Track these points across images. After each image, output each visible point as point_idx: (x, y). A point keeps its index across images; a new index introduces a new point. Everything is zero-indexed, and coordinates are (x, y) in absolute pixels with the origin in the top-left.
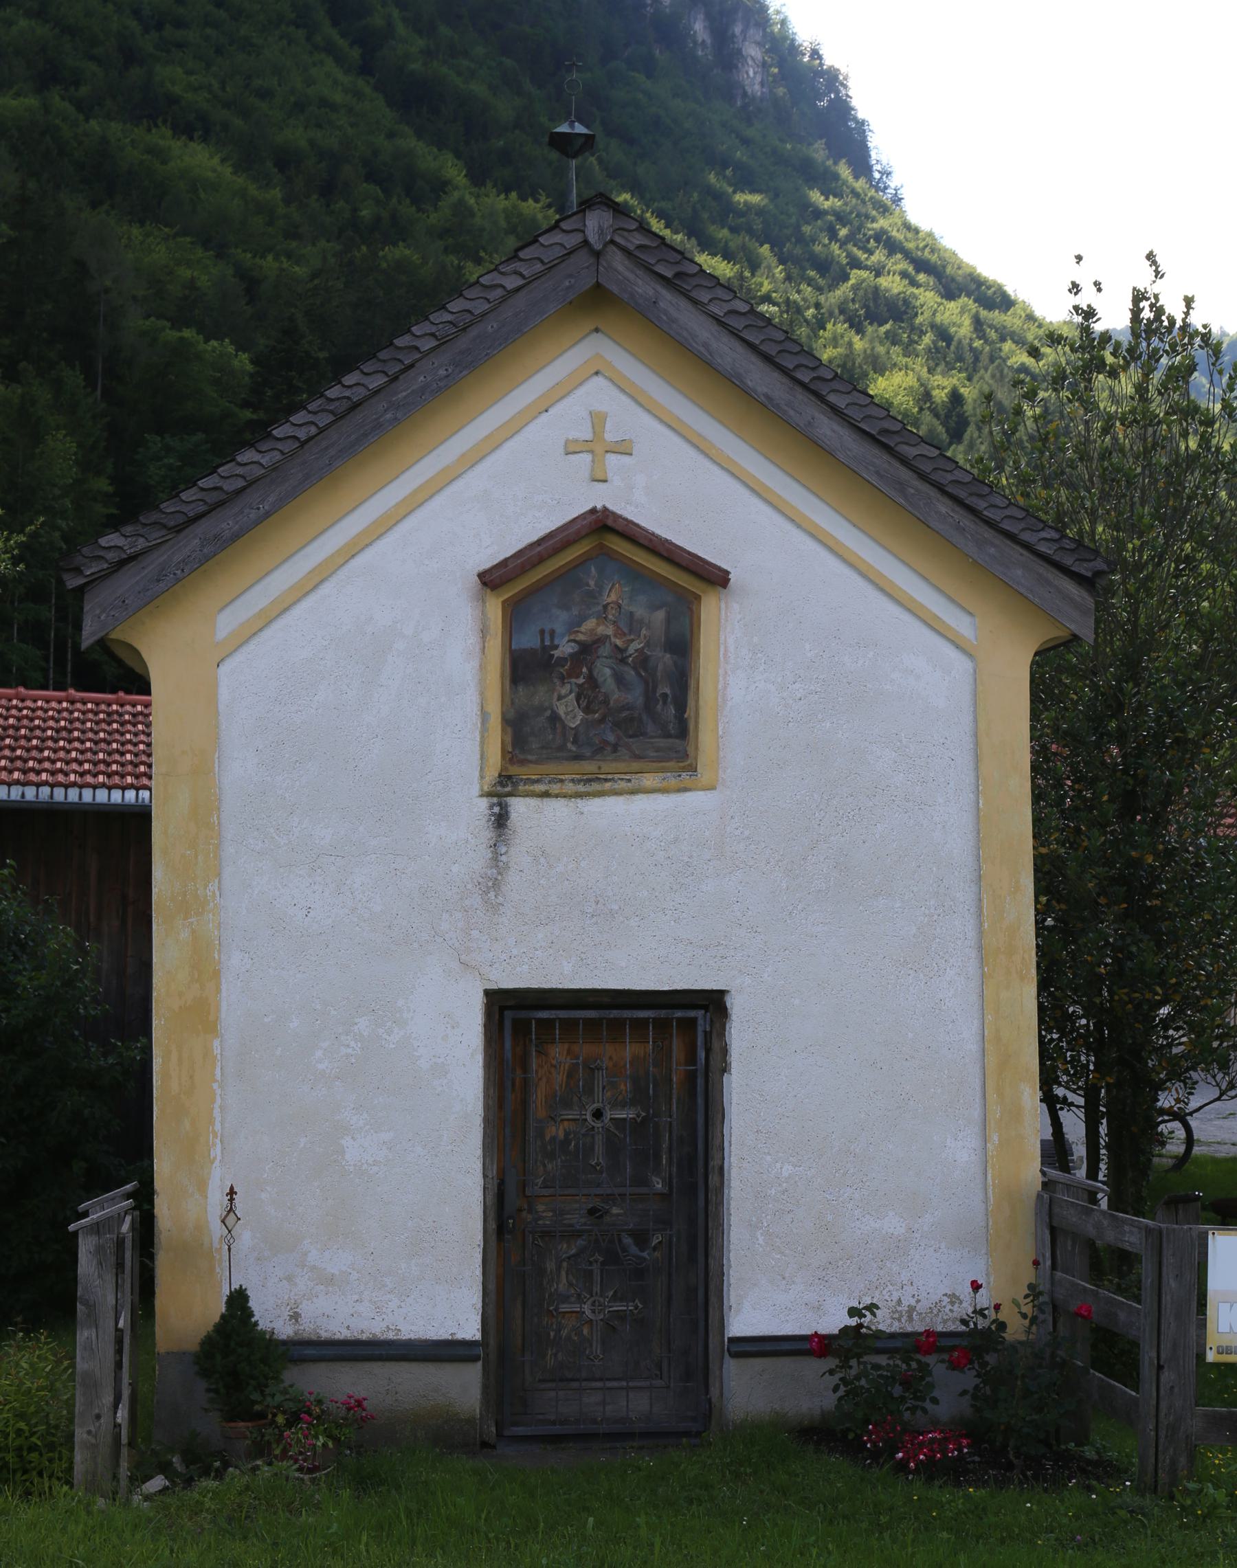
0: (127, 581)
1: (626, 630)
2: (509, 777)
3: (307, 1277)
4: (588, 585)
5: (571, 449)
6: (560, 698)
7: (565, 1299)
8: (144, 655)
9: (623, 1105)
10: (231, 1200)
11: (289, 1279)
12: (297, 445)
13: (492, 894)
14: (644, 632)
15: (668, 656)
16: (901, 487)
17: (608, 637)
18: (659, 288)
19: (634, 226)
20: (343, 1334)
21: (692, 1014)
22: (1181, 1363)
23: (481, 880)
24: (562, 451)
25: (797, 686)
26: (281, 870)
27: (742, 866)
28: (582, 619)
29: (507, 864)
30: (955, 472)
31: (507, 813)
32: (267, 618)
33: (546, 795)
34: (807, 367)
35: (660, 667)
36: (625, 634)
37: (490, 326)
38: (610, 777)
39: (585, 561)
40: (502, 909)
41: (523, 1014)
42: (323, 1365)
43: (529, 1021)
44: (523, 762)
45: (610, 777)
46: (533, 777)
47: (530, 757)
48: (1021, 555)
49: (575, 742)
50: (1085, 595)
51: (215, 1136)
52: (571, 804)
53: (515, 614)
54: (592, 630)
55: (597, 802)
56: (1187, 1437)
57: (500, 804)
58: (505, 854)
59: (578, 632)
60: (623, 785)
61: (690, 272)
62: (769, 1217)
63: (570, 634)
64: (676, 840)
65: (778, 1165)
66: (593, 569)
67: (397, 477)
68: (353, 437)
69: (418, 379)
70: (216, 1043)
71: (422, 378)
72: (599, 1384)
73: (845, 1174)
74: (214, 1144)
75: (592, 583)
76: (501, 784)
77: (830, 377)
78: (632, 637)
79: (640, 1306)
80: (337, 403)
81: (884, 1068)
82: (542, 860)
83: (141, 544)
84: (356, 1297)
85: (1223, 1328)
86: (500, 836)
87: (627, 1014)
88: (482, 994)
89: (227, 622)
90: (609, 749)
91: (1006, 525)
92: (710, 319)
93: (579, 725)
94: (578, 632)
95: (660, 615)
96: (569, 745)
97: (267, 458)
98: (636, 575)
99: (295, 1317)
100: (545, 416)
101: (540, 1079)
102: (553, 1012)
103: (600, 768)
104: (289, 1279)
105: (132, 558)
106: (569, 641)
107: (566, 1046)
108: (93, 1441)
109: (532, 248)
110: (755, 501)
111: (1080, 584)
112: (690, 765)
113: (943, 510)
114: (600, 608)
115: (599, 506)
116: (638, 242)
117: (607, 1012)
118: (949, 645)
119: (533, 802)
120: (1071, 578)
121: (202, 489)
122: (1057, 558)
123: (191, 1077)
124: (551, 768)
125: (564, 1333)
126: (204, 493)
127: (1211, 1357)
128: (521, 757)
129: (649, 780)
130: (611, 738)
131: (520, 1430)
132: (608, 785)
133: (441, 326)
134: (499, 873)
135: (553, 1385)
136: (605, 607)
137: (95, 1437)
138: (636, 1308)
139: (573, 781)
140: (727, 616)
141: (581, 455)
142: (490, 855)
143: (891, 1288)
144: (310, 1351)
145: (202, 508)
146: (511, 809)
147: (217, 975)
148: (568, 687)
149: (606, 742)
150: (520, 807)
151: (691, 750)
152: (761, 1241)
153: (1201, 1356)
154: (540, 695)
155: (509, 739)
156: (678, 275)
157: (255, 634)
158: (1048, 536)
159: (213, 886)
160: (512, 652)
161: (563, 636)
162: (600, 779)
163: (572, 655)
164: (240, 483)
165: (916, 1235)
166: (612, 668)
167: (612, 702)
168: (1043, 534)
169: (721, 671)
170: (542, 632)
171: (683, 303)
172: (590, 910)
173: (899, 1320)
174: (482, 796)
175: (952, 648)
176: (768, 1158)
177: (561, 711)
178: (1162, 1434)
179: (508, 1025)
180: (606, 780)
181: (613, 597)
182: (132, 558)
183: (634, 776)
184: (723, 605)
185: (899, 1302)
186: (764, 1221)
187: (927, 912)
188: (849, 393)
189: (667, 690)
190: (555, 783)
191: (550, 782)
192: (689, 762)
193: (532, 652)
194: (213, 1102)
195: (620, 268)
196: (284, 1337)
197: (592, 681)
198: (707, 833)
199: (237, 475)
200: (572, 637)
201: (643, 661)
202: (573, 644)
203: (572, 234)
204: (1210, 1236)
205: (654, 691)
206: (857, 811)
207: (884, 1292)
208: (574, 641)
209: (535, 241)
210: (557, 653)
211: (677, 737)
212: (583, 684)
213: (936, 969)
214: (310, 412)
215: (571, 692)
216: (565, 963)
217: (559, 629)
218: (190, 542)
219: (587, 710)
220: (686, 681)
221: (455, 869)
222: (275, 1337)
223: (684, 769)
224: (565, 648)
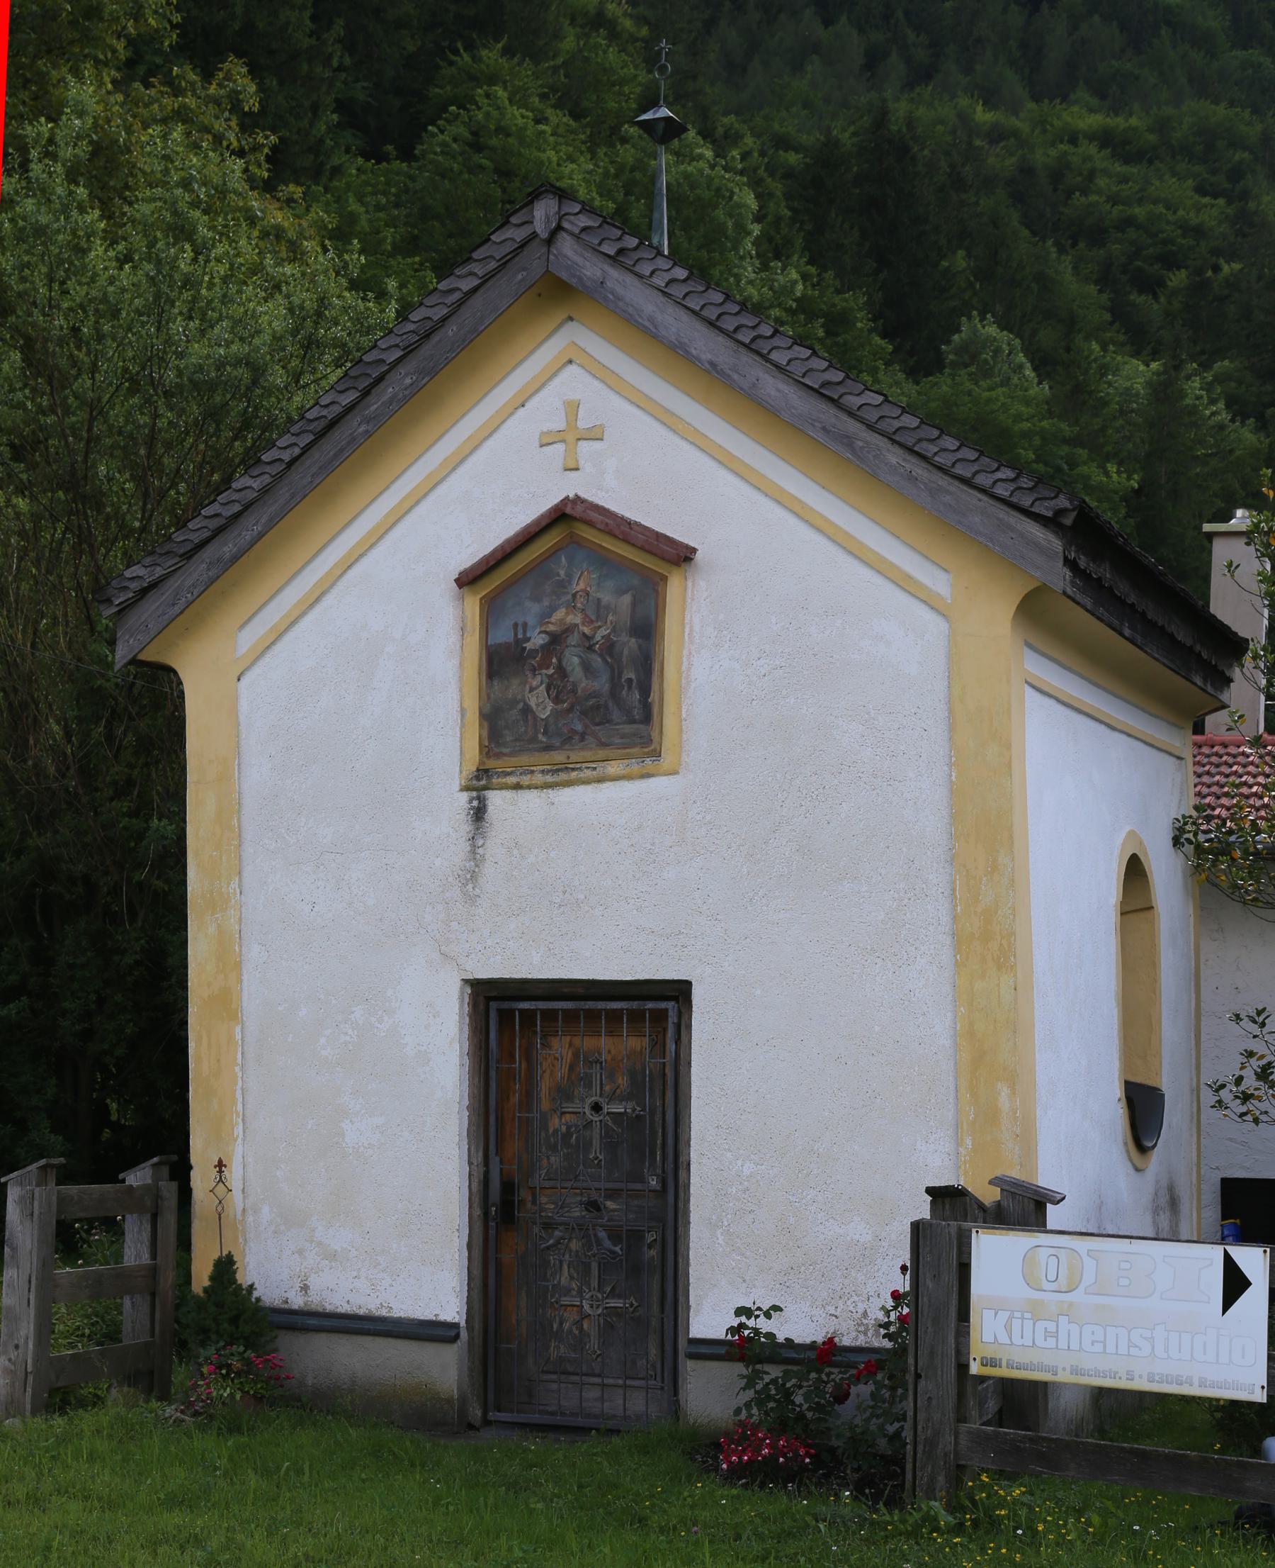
0: (150, 608)
1: (593, 618)
2: (486, 771)
3: (314, 1251)
4: (559, 575)
5: (544, 442)
6: (531, 690)
7: (568, 1291)
8: (181, 675)
9: (622, 1099)
10: (220, 1172)
11: (300, 1252)
12: (284, 466)
13: (470, 886)
14: (610, 618)
15: (633, 640)
16: (847, 441)
17: (577, 625)
18: (607, 268)
19: (577, 208)
20: (344, 1308)
21: (663, 1005)
22: (940, 1373)
23: (460, 872)
24: (537, 444)
25: (762, 661)
26: (291, 868)
27: (702, 851)
28: (553, 609)
29: (483, 856)
30: (902, 418)
31: (485, 806)
32: (278, 635)
33: (518, 787)
34: (747, 327)
35: (626, 652)
36: (592, 622)
37: (451, 330)
38: (578, 766)
39: (557, 551)
40: (479, 901)
41: (506, 1005)
42: (323, 1336)
43: (513, 1011)
44: (498, 756)
45: (578, 766)
46: (508, 770)
47: (505, 750)
48: (980, 500)
49: (545, 733)
50: (1051, 537)
51: (238, 1116)
52: (543, 795)
53: (491, 610)
54: (562, 620)
55: (567, 792)
56: (946, 1454)
57: (478, 798)
58: (482, 846)
59: (548, 623)
60: (588, 773)
61: (630, 247)
62: (729, 1216)
63: (541, 625)
64: (640, 827)
65: (739, 1163)
66: (563, 559)
67: (388, 487)
68: (331, 453)
69: (388, 391)
70: (238, 1029)
71: (391, 390)
72: (597, 1380)
73: (808, 1175)
74: (237, 1123)
75: (562, 573)
76: (478, 778)
77: (769, 334)
78: (599, 624)
79: (636, 1304)
80: (316, 423)
81: (849, 1063)
82: (515, 852)
83: (159, 572)
84: (355, 1274)
85: (987, 1337)
86: (478, 829)
87: (601, 1005)
88: (459, 984)
89: (248, 639)
90: (577, 737)
91: (959, 470)
92: (656, 291)
93: (548, 716)
94: (548, 623)
95: (627, 599)
96: (540, 736)
97: (258, 482)
98: (606, 563)
99: (305, 1288)
100: (522, 411)
101: (544, 1072)
102: (533, 1003)
103: (568, 757)
104: (300, 1252)
105: (153, 586)
106: (540, 632)
107: (568, 1038)
108: (13, 1368)
109: (486, 247)
110: (723, 473)
111: (1045, 526)
112: (655, 750)
113: (893, 460)
114: (570, 597)
115: (571, 496)
116: (583, 225)
117: (583, 1003)
118: (923, 606)
119: (508, 794)
120: (1035, 521)
121: (206, 517)
122: (1014, 500)
123: (218, 1061)
124: (524, 759)
125: (566, 1326)
126: (207, 521)
127: (975, 1369)
128: (497, 750)
129: (613, 768)
130: (579, 727)
131: (503, 1416)
132: (574, 774)
133: (405, 337)
134: (477, 866)
135: (554, 1377)
136: (574, 595)
137: (14, 1364)
138: (632, 1305)
139: (543, 772)
140: (693, 594)
141: (555, 445)
142: (469, 848)
143: (855, 1298)
144: (313, 1322)
145: (206, 534)
146: (489, 803)
147: (238, 966)
148: (539, 678)
149: (575, 732)
150: (497, 800)
151: (655, 735)
152: (721, 1241)
153: (963, 1367)
154: (514, 688)
155: (485, 734)
156: (621, 251)
157: (268, 648)
158: (1004, 477)
159: (234, 884)
160: (488, 648)
161: (534, 628)
162: (567, 768)
163: (542, 646)
164: (237, 508)
165: (883, 1244)
166: (580, 657)
167: (579, 691)
168: (999, 475)
169: (685, 652)
170: (516, 625)
171: (629, 279)
172: (558, 900)
173: (865, 1334)
174: (461, 790)
175: (927, 608)
176: (729, 1154)
177: (533, 702)
178: (920, 1448)
179: (493, 1015)
180: (573, 769)
181: (582, 586)
182: (153, 586)
183: (601, 764)
184: (690, 584)
185: (865, 1314)
186: (725, 1220)
187: (896, 896)
188: (789, 348)
189: (632, 676)
190: (526, 774)
191: (521, 774)
192: (652, 747)
193: (507, 646)
194: (236, 1084)
195: (570, 253)
196: (296, 1307)
197: (562, 672)
198: (669, 820)
199: (233, 501)
200: (543, 629)
201: (610, 647)
202: (544, 635)
203: (523, 228)
204: (974, 1234)
205: (620, 677)
206: (821, 790)
207: (849, 1303)
208: (545, 632)
209: (488, 240)
210: (529, 646)
211: (641, 722)
212: (553, 674)
213: (905, 957)
214: (293, 435)
215: (542, 683)
216: (534, 953)
217: (531, 621)
218: (198, 569)
219: (557, 700)
220: (651, 664)
221: (438, 862)
222: (261, 1304)
223: (649, 755)
224: (537, 640)
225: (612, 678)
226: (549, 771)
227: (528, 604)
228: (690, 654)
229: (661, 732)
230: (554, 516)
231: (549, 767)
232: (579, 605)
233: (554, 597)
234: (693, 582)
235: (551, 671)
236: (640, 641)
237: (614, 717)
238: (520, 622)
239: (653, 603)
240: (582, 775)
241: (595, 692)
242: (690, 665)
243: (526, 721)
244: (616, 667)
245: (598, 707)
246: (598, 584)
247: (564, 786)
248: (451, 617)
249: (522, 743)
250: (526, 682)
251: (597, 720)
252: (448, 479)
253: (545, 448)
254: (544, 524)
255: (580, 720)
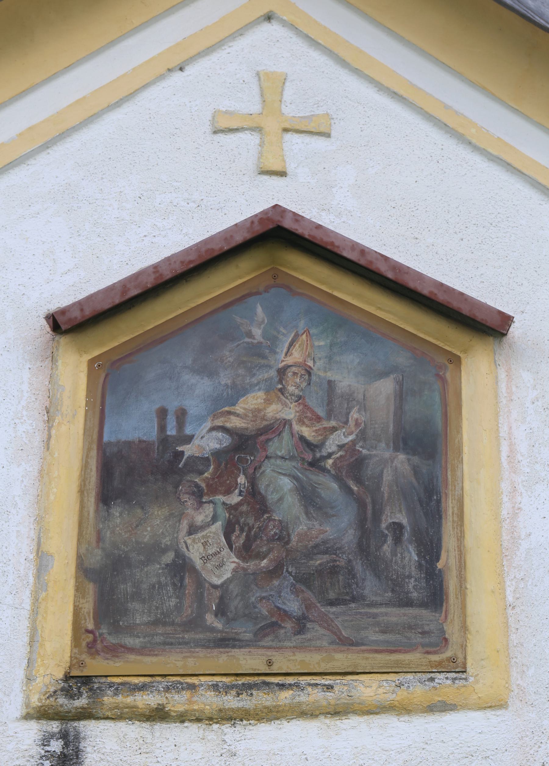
2: (87, 680)
5: (223, 124)
6: (193, 530)
14: (354, 415)
15: (402, 457)
17: (286, 423)
24: (208, 128)
31: (78, 752)
35: (387, 476)
36: (319, 419)
38: (290, 680)
39: (250, 295)
46: (135, 680)
47: (129, 641)
49: (221, 612)
52: (211, 735)
57: (64, 736)
59: (229, 413)
63: (215, 417)
75: (257, 332)
78: (333, 423)
90: (289, 625)
94: (229, 413)
96: (210, 619)
103: (270, 663)
106: (213, 429)
112: (453, 660)
114: (273, 373)
128: (112, 640)
132: (285, 696)
136: (282, 372)
139: (215, 687)
148: (209, 510)
149: (285, 615)
155: (88, 606)
160: (102, 447)
161: (201, 419)
162: (267, 684)
163: (217, 454)
166: (295, 478)
167: (294, 539)
169: (505, 486)
170: (162, 413)
174: (27, 717)
180: (282, 686)
181: (297, 356)
191: (167, 689)
192: (449, 654)
200: (219, 422)
202: (220, 435)
211: (423, 605)
212: (239, 504)
215: (215, 519)
220: (439, 502)
225: (361, 522)
226: (228, 688)
227: (188, 378)
228: (515, 489)
229: (464, 628)
230: (259, 229)
231: (225, 679)
232: (291, 388)
233: (241, 371)
234: (509, 376)
235: (234, 499)
236: (416, 460)
237: (366, 592)
238: (172, 406)
239: (437, 399)
240: (303, 698)
241: (324, 542)
242: (516, 512)
243: (179, 587)
244: (369, 500)
245: (334, 571)
246: (330, 359)
247: (260, 719)
248: (25, 387)
249: (169, 629)
250: (181, 516)
251: (332, 595)
252: (32, 161)
253: (221, 137)
254: (239, 239)
255: (296, 592)
